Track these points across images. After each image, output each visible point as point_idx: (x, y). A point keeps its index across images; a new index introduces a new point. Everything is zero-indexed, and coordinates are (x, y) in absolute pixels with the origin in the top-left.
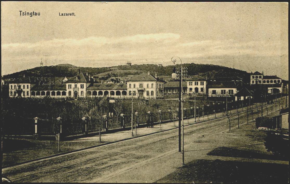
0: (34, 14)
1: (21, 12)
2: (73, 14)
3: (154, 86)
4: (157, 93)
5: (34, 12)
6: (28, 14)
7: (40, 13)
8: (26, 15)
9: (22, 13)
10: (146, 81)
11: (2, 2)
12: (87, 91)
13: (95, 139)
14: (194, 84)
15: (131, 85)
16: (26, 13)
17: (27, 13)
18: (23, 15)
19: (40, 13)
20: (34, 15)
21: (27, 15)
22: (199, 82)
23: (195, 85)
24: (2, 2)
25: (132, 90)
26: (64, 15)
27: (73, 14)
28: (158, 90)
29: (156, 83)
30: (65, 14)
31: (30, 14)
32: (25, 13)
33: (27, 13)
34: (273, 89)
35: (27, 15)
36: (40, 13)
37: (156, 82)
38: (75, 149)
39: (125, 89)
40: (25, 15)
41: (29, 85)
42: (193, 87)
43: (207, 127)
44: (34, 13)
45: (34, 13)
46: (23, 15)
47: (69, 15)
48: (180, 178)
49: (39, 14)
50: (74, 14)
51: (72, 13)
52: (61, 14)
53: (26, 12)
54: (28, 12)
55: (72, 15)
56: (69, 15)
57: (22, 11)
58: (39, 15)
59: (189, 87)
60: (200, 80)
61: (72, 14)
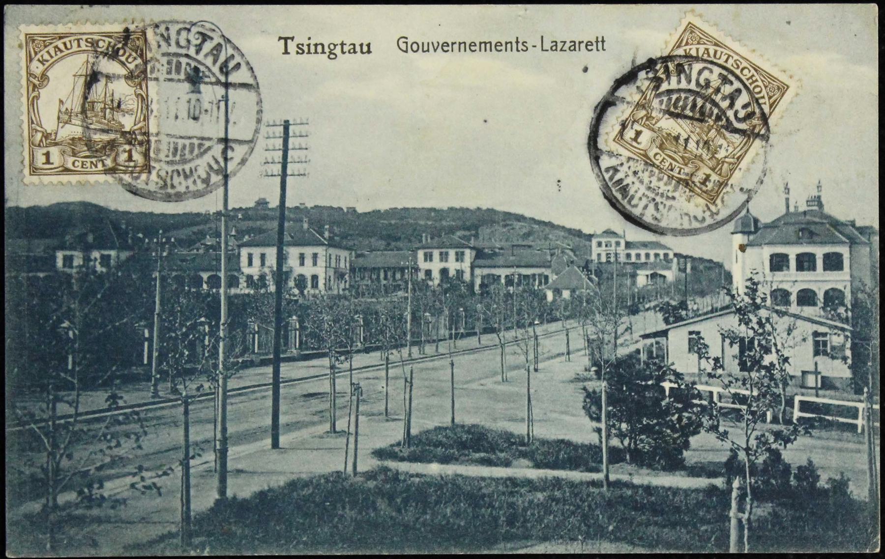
0: (346, 49)
1: (289, 41)
2: (600, 44)
3: (321, 262)
4: (330, 280)
10: (788, 243)
11: (874, 8)
12: (229, 273)
14: (311, 264)
15: (267, 256)
18: (300, 51)
21: (486, 50)
22: (452, 253)
23: (441, 260)
24: (874, 8)
25: (254, 271)
26: (560, 46)
27: (600, 44)
28: (331, 273)
29: (324, 253)
33: (316, 45)
37: (324, 248)
39: (236, 270)
41: (320, 251)
42: (436, 266)
44: (517, 42)
45: (517, 42)
47: (583, 46)
48: (780, 523)
50: (603, 41)
51: (594, 40)
52: (547, 46)
55: (594, 47)
56: (583, 46)
57: (292, 39)
59: (423, 265)
60: (451, 246)
61: (597, 42)
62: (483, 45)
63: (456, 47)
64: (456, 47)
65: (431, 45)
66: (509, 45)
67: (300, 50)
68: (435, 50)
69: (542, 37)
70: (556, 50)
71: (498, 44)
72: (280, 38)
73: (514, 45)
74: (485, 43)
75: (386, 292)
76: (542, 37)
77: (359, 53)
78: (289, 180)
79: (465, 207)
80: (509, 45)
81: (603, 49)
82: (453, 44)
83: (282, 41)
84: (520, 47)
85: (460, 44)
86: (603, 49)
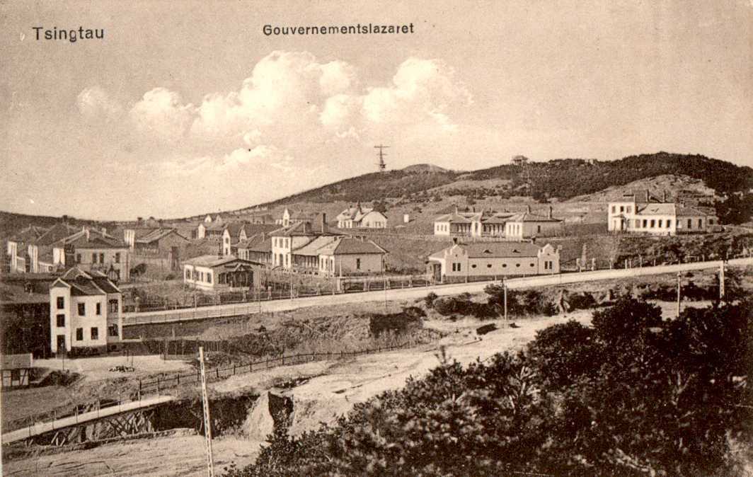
0: (84, 34)
1: (40, 30)
5: (359, 25)
6: (63, 33)
7: (102, 31)
8: (55, 38)
9: (42, 33)
13: (17, 435)
15: (122, 255)
16: (55, 31)
17: (60, 32)
19: (102, 31)
20: (81, 38)
21: (60, 38)
26: (381, 29)
30: (385, 27)
31: (281, 30)
32: (53, 31)
34: (49, 355)
35: (60, 38)
36: (104, 33)
38: (574, 201)
40: (53, 37)
43: (47, 450)
46: (49, 33)
49: (99, 35)
53: (55, 28)
54: (62, 29)
57: (42, 28)
58: (102, 36)
62: (332, 30)
63: (310, 31)
64: (310, 31)
65: (290, 30)
66: (352, 30)
67: (48, 35)
68: (293, 33)
69: (38, 38)
70: (379, 32)
71: (323, 29)
72: (34, 28)
73: (357, 29)
74: (334, 29)
75: (232, 351)
76: (38, 38)
77: (85, 38)
78: (540, 273)
79: (633, 155)
80: (352, 30)
81: (412, 32)
82: (308, 28)
83: (35, 30)
84: (361, 30)
85: (313, 28)
86: (412, 32)
